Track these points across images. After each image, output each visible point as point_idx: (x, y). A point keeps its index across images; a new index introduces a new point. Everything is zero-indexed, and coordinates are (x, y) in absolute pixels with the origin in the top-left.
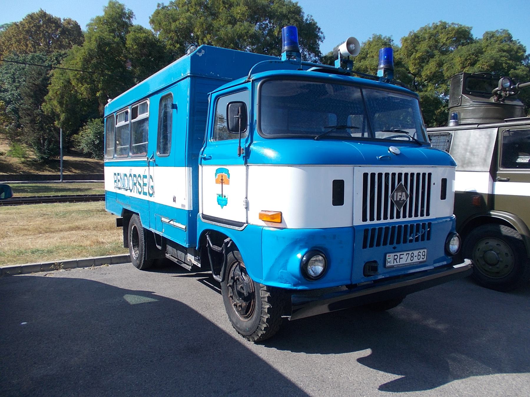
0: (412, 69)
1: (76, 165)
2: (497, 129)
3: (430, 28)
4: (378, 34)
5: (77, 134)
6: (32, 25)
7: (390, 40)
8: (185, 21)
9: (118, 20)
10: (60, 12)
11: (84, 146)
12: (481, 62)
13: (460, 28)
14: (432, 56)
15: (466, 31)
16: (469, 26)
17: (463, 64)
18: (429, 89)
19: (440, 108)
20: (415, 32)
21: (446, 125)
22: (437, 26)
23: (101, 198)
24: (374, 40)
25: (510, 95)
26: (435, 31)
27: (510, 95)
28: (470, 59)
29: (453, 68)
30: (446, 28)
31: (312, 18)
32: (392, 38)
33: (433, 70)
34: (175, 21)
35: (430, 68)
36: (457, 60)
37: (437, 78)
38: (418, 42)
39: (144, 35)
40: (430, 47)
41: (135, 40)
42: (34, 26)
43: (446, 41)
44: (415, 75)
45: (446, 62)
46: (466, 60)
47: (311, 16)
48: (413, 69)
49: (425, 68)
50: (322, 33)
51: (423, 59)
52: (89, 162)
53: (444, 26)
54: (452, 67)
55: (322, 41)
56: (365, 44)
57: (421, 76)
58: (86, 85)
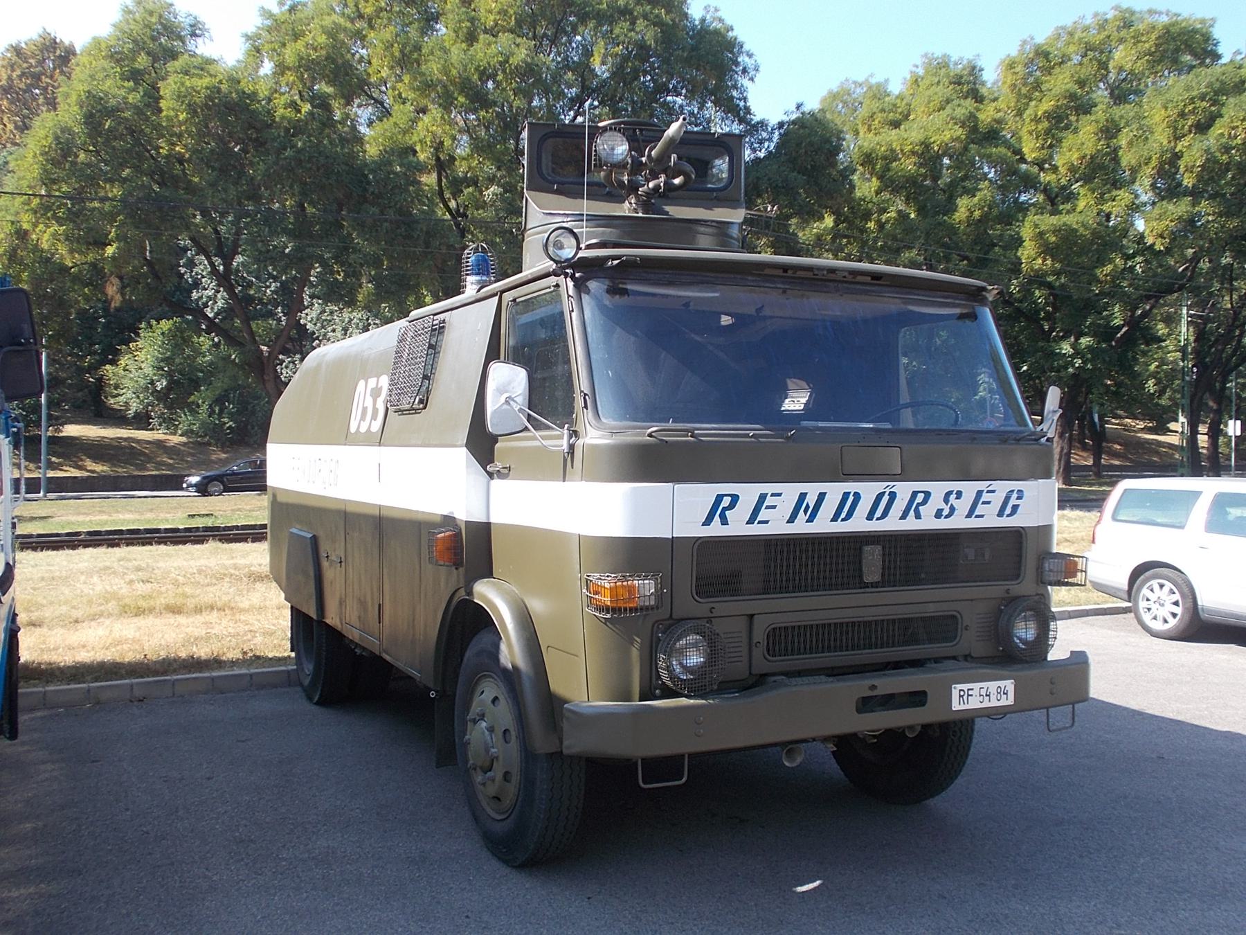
0: (1030, 148)
1: (98, 450)
3: (1086, 29)
4: (938, 54)
5: (114, 362)
6: (18, 72)
7: (974, 70)
8: (322, 39)
9: (155, 45)
10: (65, 36)
11: (128, 398)
12: (1226, 119)
14: (1085, 108)
15: (1195, 31)
16: (1208, 16)
17: (1176, 129)
18: (1081, 204)
20: (1040, 39)
21: (457, 290)
22: (1106, 20)
23: (14, 551)
24: (927, 72)
27: (669, 186)
28: (1193, 112)
29: (1147, 138)
31: (719, 14)
33: (1089, 149)
34: (296, 36)
35: (1082, 141)
37: (1103, 172)
38: (1048, 71)
39: (206, 81)
41: (180, 97)
42: (23, 74)
44: (1040, 164)
45: (1127, 124)
46: (1182, 115)
47: (716, 10)
50: (750, 56)
51: (1059, 119)
52: (138, 441)
53: (1126, 21)
54: (1143, 136)
55: (752, 79)
57: (1055, 169)
58: (55, 227)
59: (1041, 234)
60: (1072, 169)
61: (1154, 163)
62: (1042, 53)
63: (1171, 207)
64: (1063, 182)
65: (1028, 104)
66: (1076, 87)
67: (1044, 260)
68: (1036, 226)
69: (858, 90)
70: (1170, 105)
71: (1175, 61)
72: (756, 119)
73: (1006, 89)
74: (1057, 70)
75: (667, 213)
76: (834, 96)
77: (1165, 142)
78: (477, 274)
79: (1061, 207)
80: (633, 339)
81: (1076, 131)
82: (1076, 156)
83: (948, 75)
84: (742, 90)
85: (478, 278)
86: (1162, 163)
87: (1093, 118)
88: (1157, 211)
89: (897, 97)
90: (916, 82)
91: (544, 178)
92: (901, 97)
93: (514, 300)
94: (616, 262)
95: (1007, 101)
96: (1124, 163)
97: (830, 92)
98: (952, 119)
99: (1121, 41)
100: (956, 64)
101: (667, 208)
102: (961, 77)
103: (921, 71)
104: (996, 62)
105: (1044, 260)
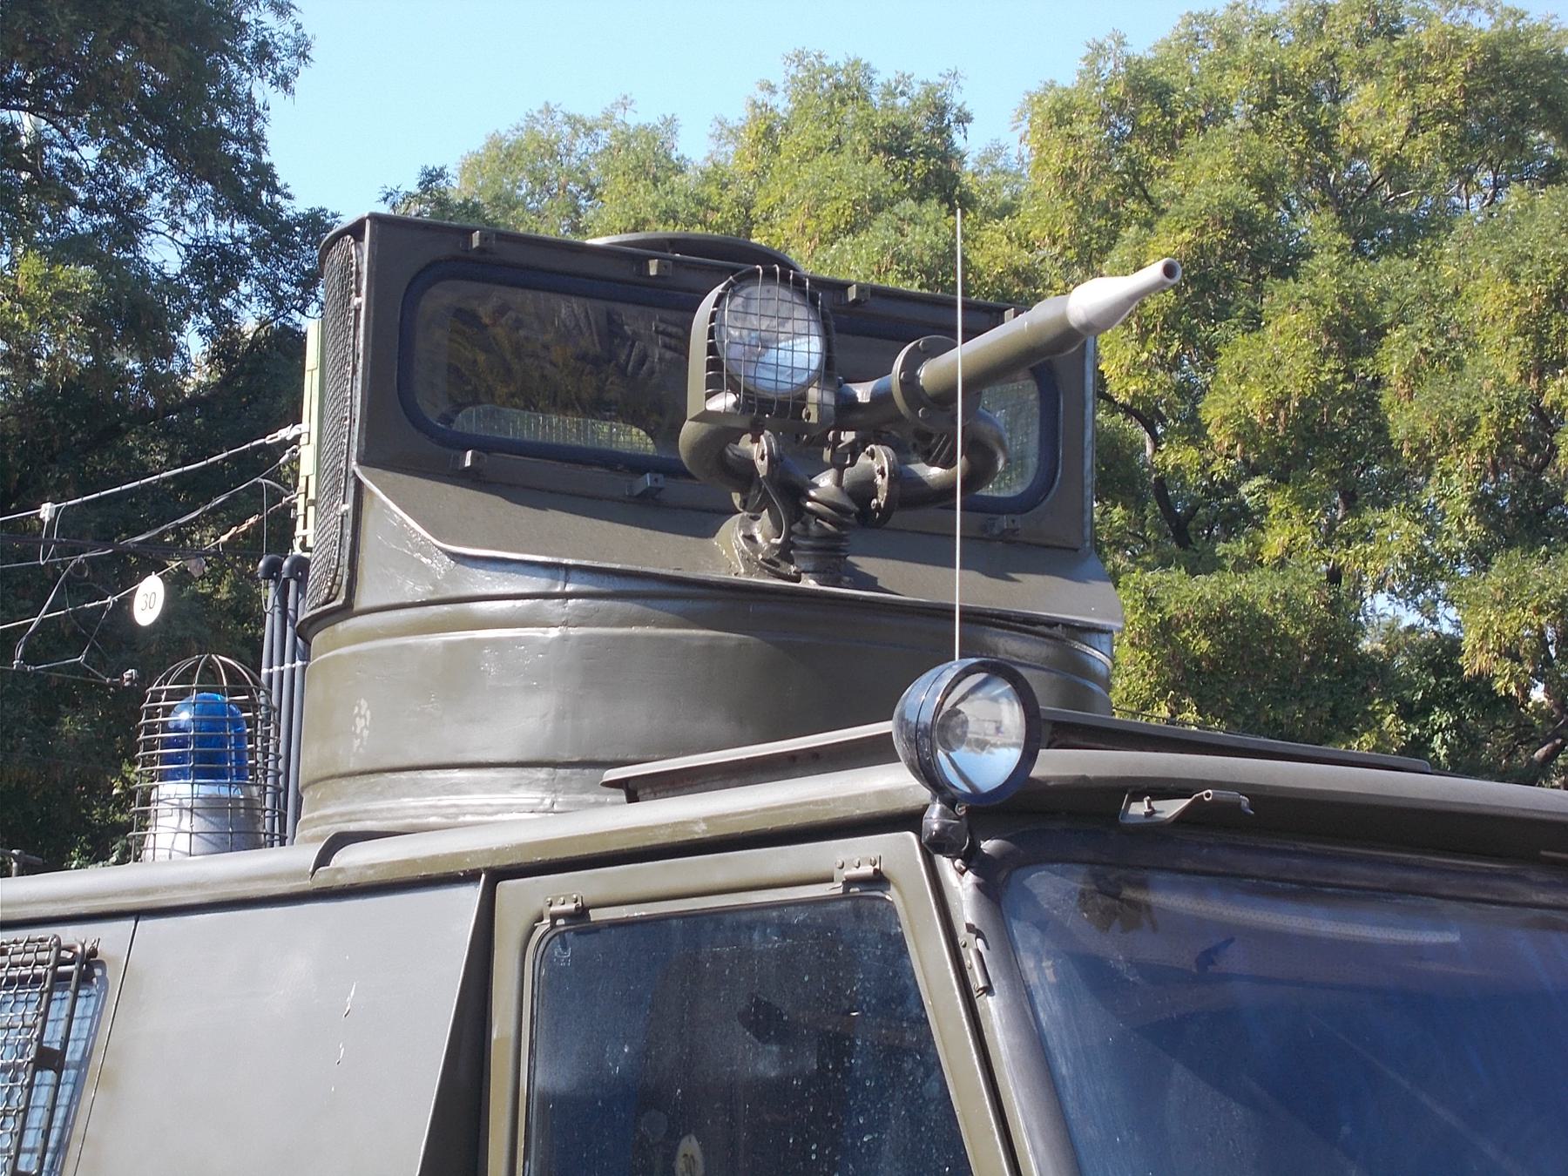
2: (471, 896)
3: (1267, 28)
4: (836, 56)
7: (941, 114)
13: (1512, 39)
17: (1541, 340)
18: (1274, 542)
19: (1372, 722)
20: (1142, 46)
21: (113, 837)
24: (802, 106)
25: (908, 492)
26: (1311, 54)
27: (908, 492)
29: (1458, 364)
30: (1391, 35)
32: (957, 99)
33: (1297, 377)
35: (1268, 363)
36: (1492, 305)
37: (1335, 452)
38: (1170, 141)
40: (1266, 185)
43: (1410, 135)
45: (1402, 319)
48: (1135, 368)
49: (1227, 361)
54: (1447, 356)
55: (284, 82)
56: (726, 132)
57: (1195, 431)
59: (1167, 628)
60: (1247, 434)
61: (1484, 435)
62: (1146, 88)
63: (1536, 570)
64: (1219, 468)
65: (1114, 236)
66: (1252, 194)
67: (1177, 708)
68: (1152, 603)
69: (582, 145)
70: (1524, 270)
71: (1517, 144)
72: (297, 205)
73: (1046, 185)
74: (1193, 141)
75: (869, 582)
76: (506, 156)
77: (1512, 377)
78: (200, 774)
79: (1221, 548)
80: (1238, 1112)
81: (1254, 322)
82: (1257, 398)
83: (867, 125)
84: (251, 112)
85: (206, 789)
86: (1506, 439)
87: (1305, 289)
88: (1497, 576)
89: (707, 178)
90: (769, 135)
91: (418, 421)
92: (718, 178)
93: (581, 913)
94: (1171, 809)
95: (1046, 218)
96: (1398, 431)
97: (495, 143)
98: (898, 258)
99: (1367, 71)
100: (890, 93)
101: (867, 565)
102: (907, 134)
103: (782, 104)
104: (1016, 100)
105: (1177, 708)
